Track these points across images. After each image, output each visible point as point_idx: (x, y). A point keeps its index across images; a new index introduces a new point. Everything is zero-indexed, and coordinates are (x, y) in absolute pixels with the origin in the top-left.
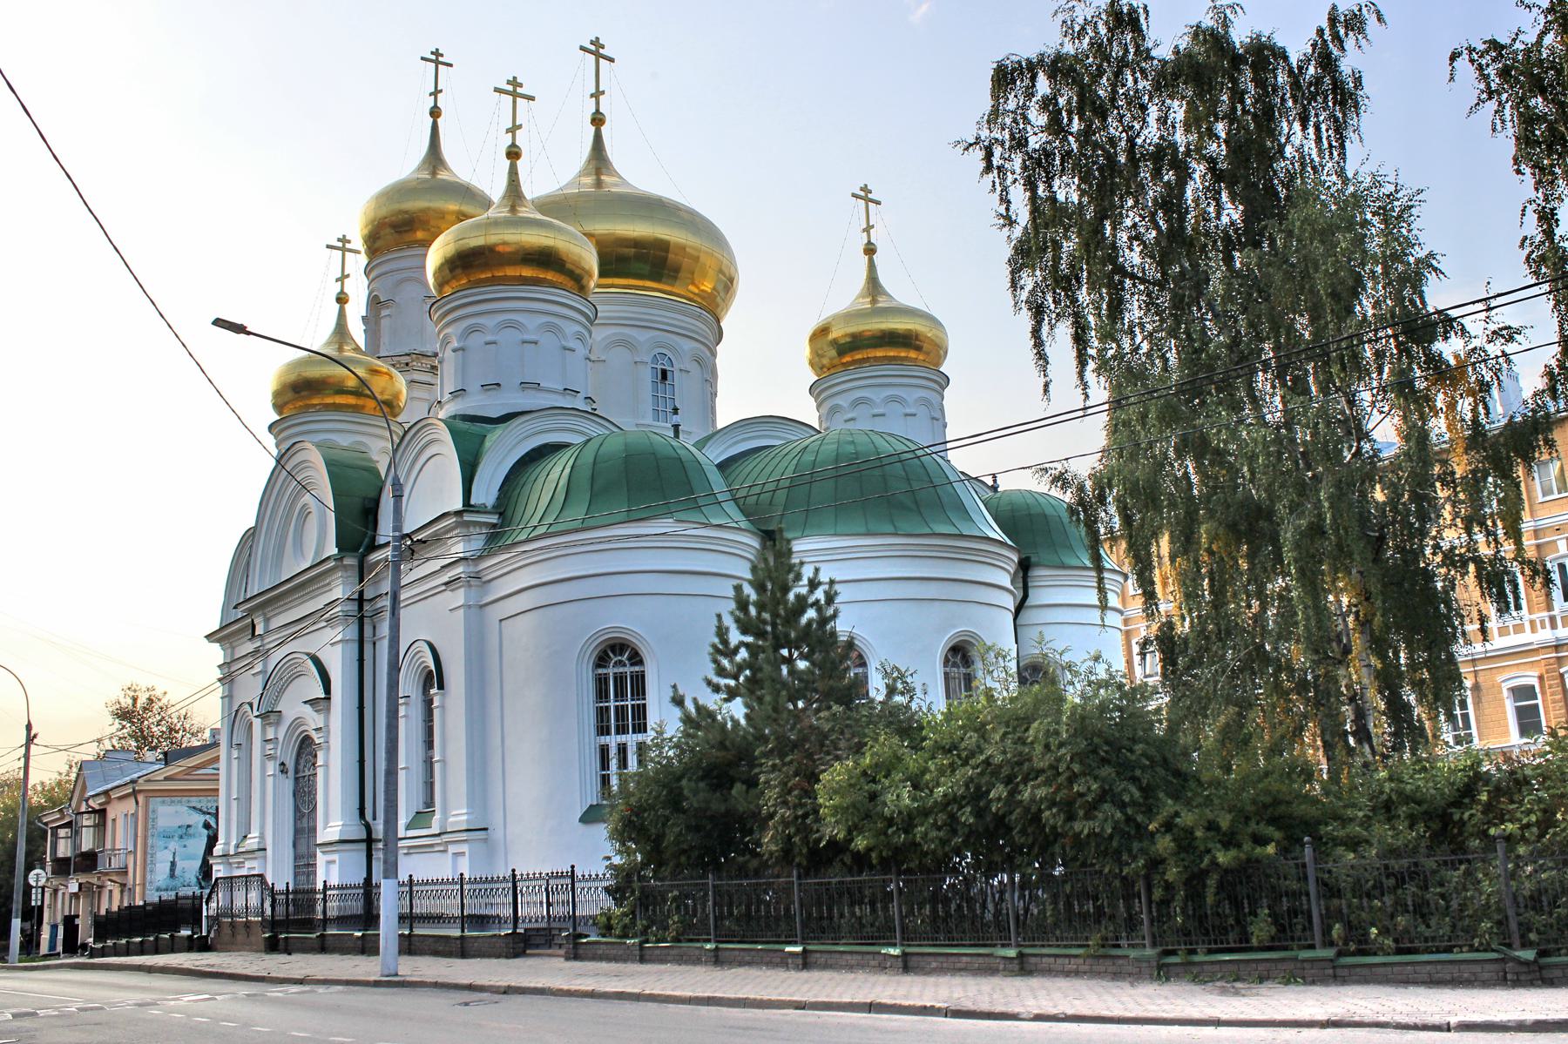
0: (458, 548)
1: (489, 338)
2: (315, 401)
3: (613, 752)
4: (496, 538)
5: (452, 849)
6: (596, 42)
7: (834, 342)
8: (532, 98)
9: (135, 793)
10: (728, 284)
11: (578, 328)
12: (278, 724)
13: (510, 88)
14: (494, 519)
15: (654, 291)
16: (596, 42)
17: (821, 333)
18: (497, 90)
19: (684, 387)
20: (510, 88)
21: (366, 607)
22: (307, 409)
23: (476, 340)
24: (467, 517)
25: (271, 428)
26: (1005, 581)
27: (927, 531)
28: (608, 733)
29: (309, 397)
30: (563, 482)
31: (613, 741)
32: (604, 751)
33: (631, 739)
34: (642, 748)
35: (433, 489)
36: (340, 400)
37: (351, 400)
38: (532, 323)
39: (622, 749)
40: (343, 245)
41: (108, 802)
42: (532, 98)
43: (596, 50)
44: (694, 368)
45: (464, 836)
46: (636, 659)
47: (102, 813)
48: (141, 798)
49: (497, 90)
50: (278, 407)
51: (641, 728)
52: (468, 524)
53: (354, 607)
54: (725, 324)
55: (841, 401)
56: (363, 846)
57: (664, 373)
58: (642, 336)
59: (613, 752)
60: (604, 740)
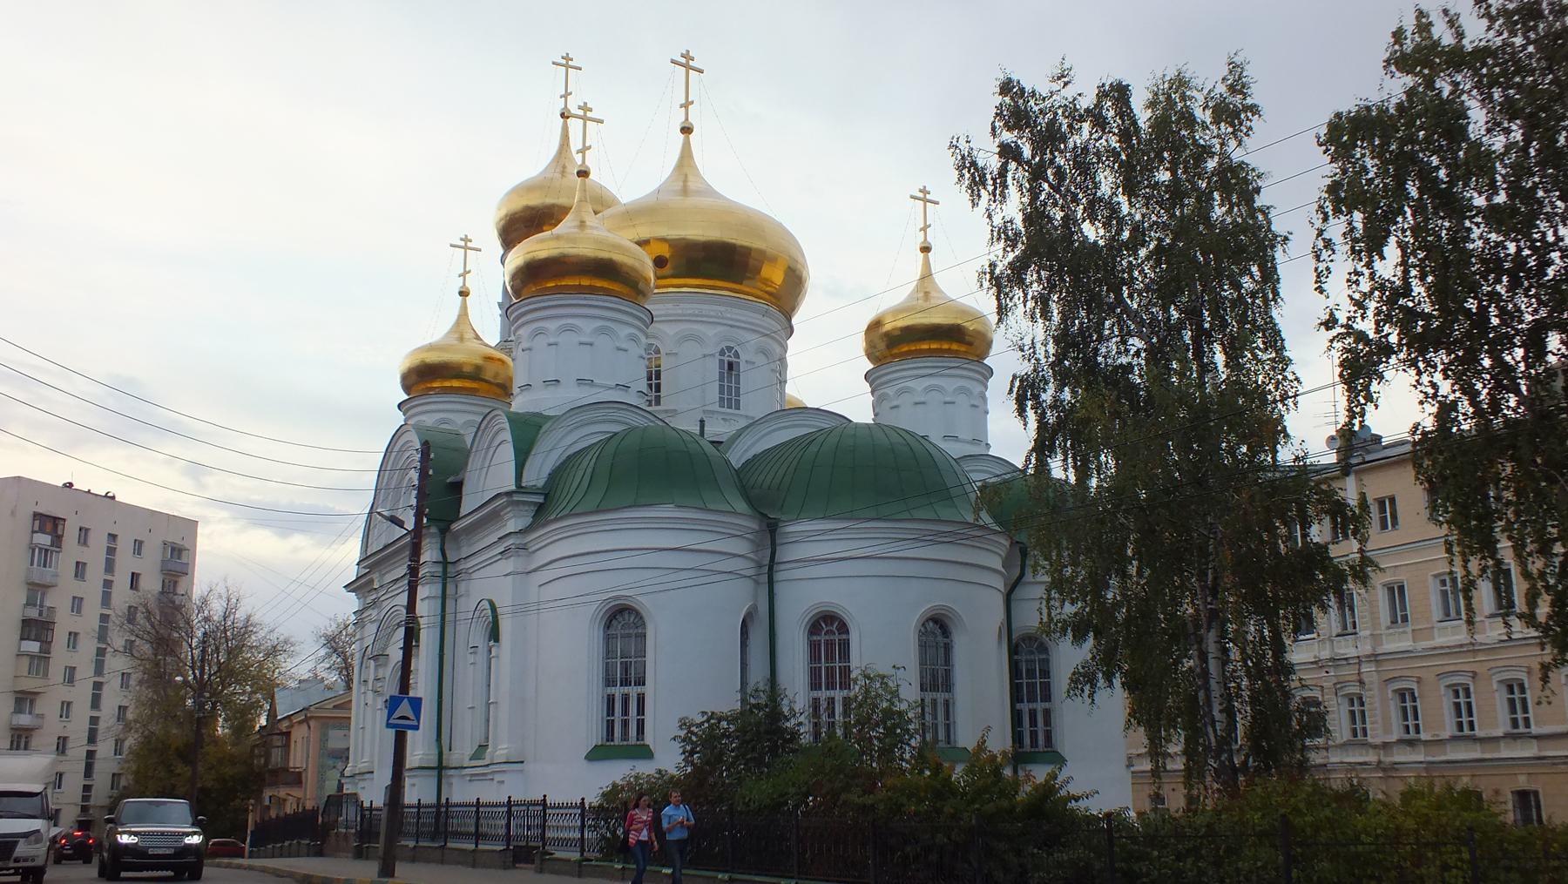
0: (512, 525)
1: (552, 340)
2: (435, 385)
3: (824, 705)
4: (541, 514)
5: (498, 777)
6: (686, 56)
7: (887, 334)
8: (601, 122)
9: (306, 720)
10: (795, 282)
11: (599, 323)
12: (385, 665)
13: (683, 60)
14: (540, 499)
15: (723, 290)
16: (686, 56)
17: (875, 325)
18: (673, 62)
19: (749, 380)
20: (683, 60)
21: (450, 569)
22: (426, 392)
23: (541, 341)
24: (516, 498)
25: (399, 406)
26: (997, 563)
27: (932, 516)
28: (834, 688)
29: (432, 381)
30: (589, 470)
31: (823, 694)
32: (610, 700)
33: (838, 695)
34: (847, 702)
35: (491, 474)
36: (456, 383)
37: (468, 384)
38: (588, 326)
39: (831, 701)
40: (466, 245)
41: (292, 726)
42: (601, 122)
43: (686, 63)
44: (760, 360)
45: (505, 767)
46: (843, 628)
47: (288, 734)
48: (312, 723)
49: (673, 62)
50: (407, 388)
51: (845, 685)
52: (519, 503)
53: (439, 569)
54: (794, 321)
55: (890, 391)
56: (435, 773)
57: (730, 365)
58: (710, 332)
59: (824, 705)
60: (611, 690)
